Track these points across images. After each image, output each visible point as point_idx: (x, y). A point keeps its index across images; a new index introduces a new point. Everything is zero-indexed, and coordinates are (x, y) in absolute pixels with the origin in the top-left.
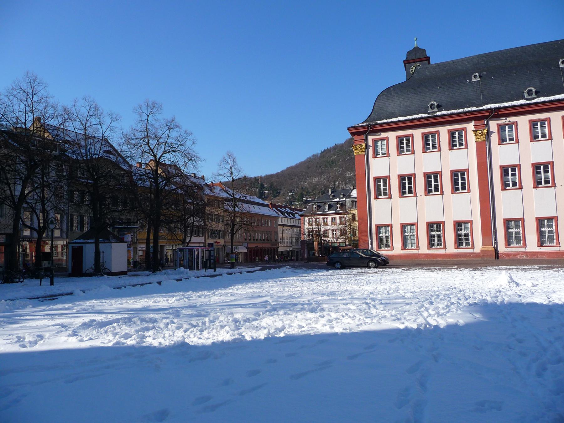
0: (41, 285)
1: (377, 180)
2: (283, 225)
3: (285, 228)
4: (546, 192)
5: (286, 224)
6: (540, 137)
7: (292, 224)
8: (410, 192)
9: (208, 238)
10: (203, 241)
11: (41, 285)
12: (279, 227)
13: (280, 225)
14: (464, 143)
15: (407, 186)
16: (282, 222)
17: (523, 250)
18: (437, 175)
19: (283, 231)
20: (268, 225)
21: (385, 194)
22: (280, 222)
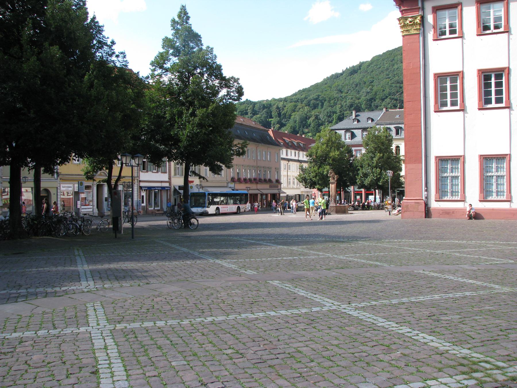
0: (133, 237)
1: (441, 77)
2: (289, 160)
3: (291, 163)
4: (496, 117)
5: (293, 157)
6: (492, 27)
7: (289, 157)
8: (499, 100)
9: (175, 174)
10: (167, 180)
11: (133, 237)
12: (283, 163)
13: (284, 159)
14: (457, 28)
15: (449, 92)
16: (287, 155)
17: (505, 206)
18: (455, 76)
19: (288, 168)
20: (266, 158)
21: (499, 100)
22: (284, 156)
